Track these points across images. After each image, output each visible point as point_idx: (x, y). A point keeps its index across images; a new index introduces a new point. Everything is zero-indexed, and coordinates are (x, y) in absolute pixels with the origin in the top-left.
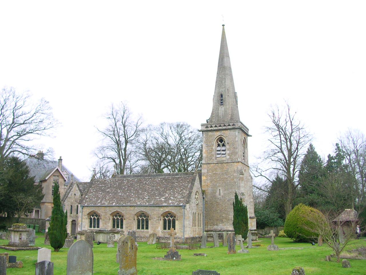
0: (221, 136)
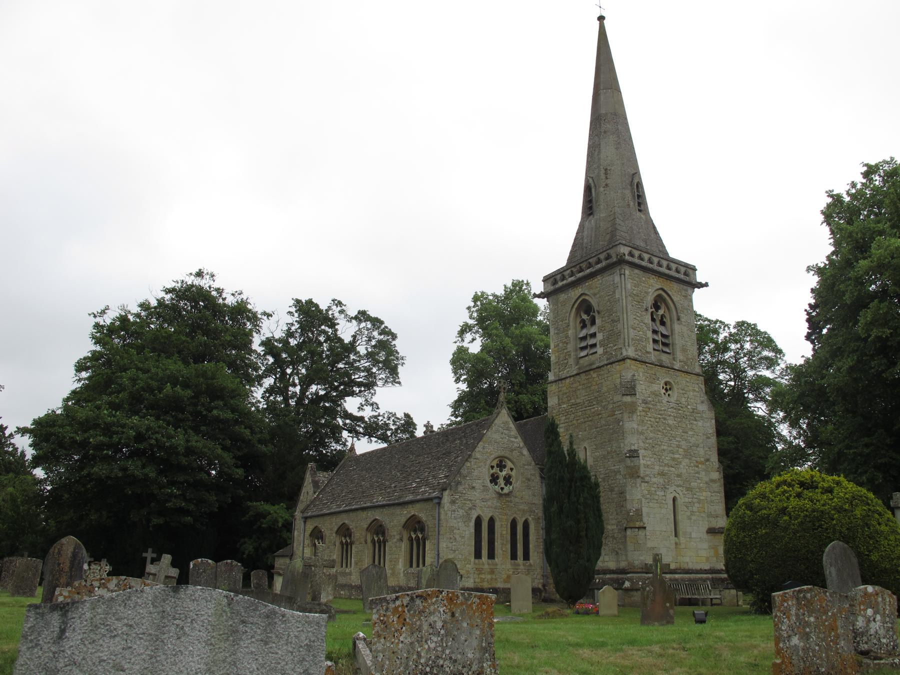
0: (583, 297)
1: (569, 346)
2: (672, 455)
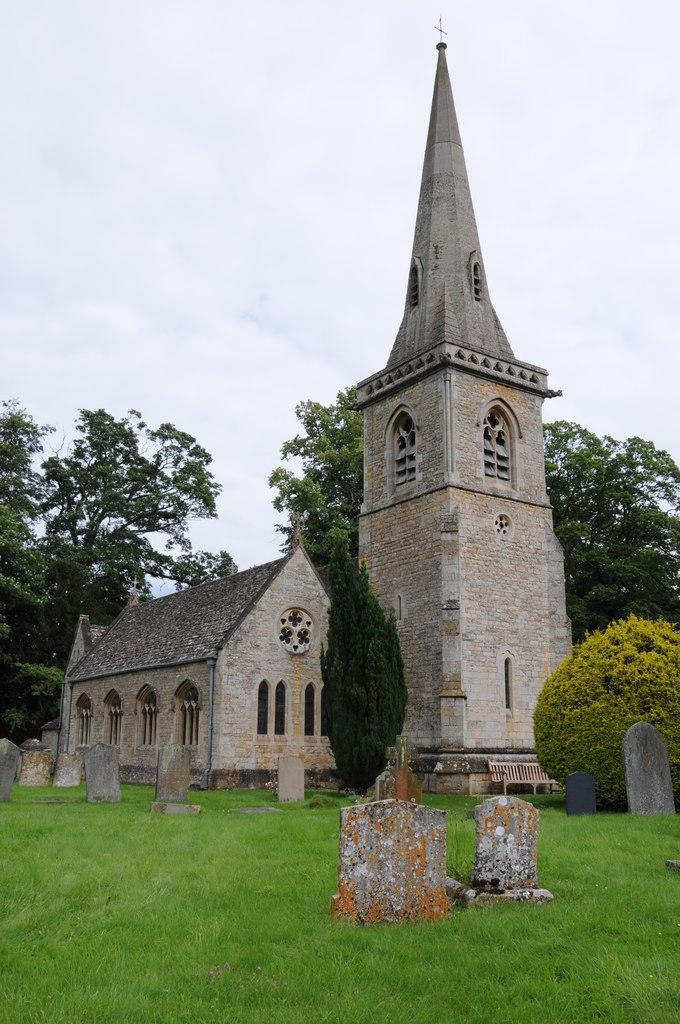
1: (384, 470)
2: (506, 607)
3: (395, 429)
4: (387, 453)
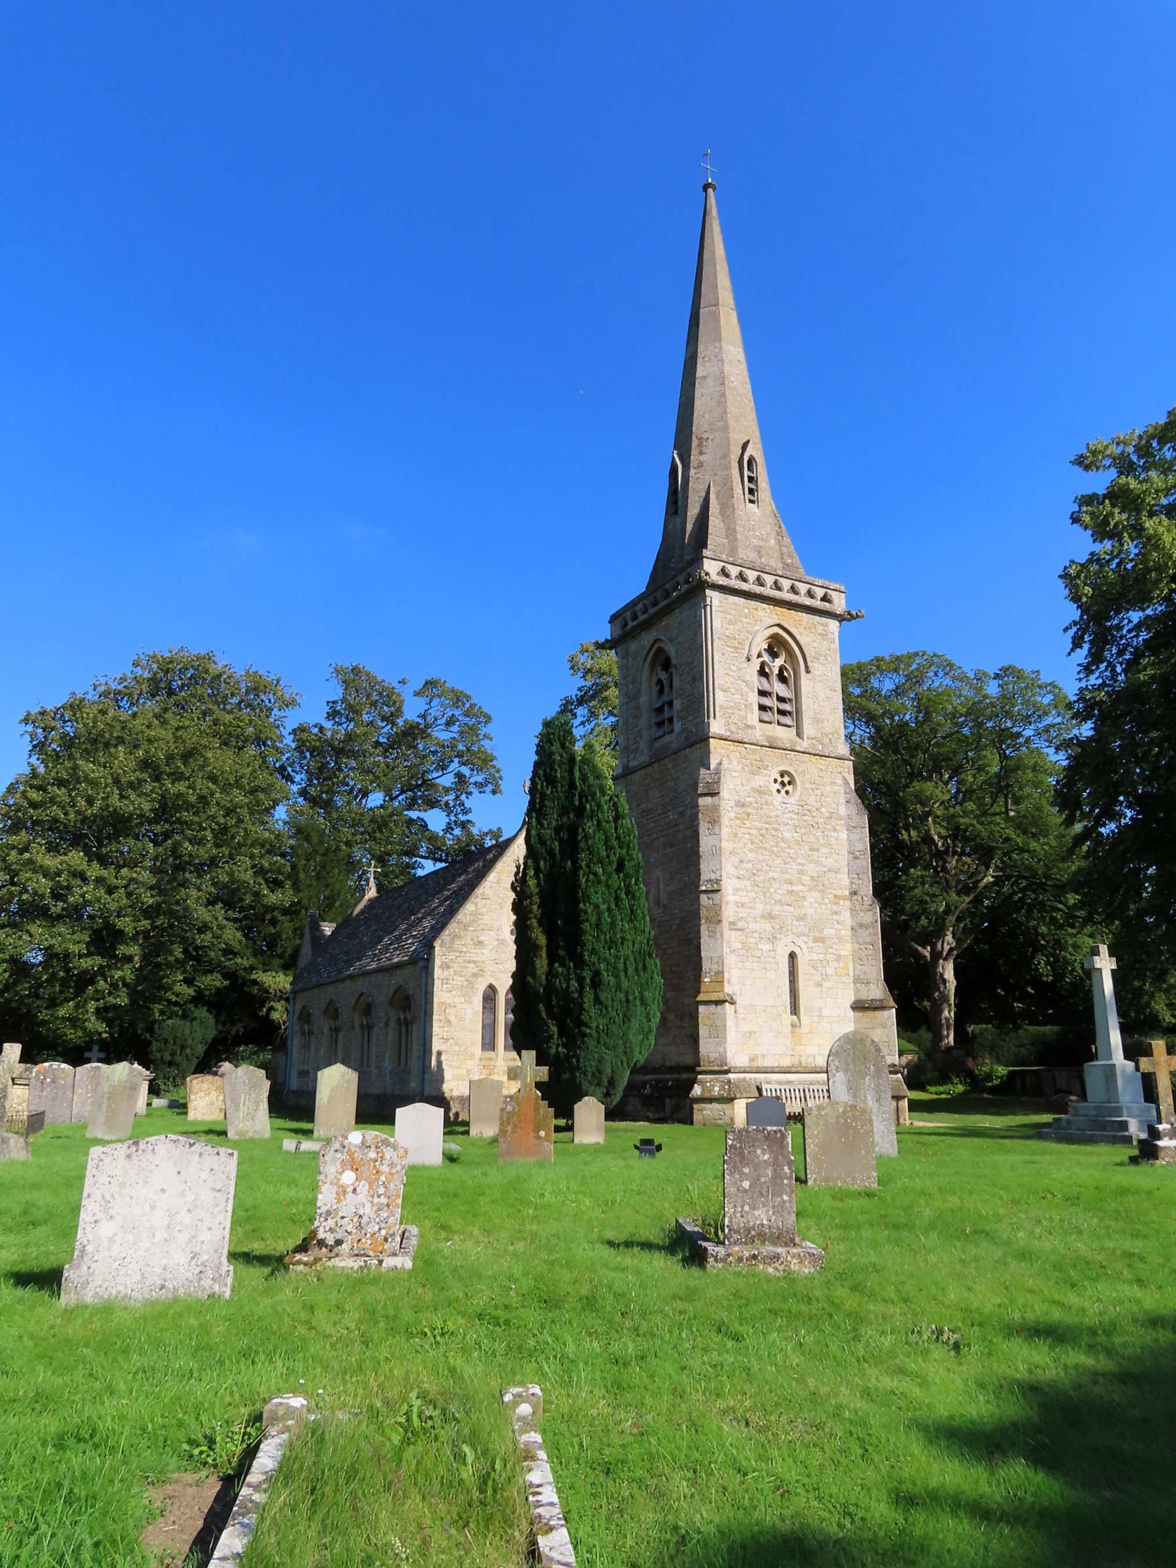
2: (789, 887)
3: (652, 671)
4: (644, 700)
